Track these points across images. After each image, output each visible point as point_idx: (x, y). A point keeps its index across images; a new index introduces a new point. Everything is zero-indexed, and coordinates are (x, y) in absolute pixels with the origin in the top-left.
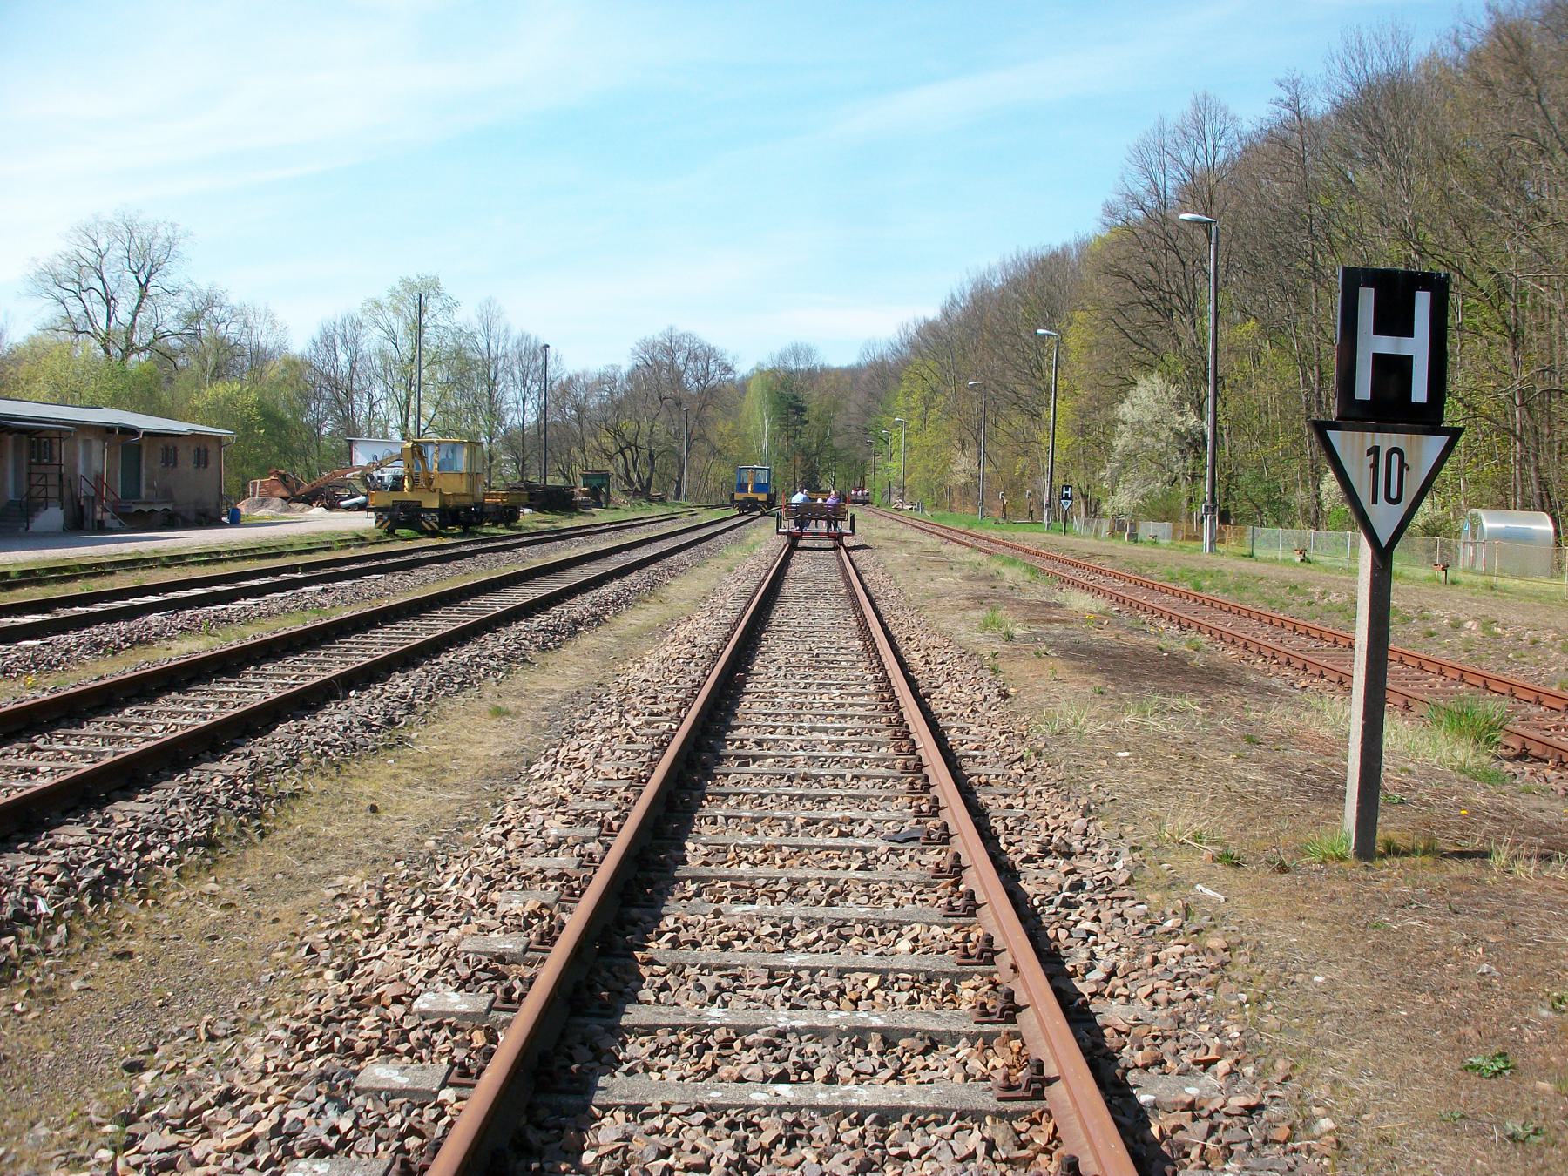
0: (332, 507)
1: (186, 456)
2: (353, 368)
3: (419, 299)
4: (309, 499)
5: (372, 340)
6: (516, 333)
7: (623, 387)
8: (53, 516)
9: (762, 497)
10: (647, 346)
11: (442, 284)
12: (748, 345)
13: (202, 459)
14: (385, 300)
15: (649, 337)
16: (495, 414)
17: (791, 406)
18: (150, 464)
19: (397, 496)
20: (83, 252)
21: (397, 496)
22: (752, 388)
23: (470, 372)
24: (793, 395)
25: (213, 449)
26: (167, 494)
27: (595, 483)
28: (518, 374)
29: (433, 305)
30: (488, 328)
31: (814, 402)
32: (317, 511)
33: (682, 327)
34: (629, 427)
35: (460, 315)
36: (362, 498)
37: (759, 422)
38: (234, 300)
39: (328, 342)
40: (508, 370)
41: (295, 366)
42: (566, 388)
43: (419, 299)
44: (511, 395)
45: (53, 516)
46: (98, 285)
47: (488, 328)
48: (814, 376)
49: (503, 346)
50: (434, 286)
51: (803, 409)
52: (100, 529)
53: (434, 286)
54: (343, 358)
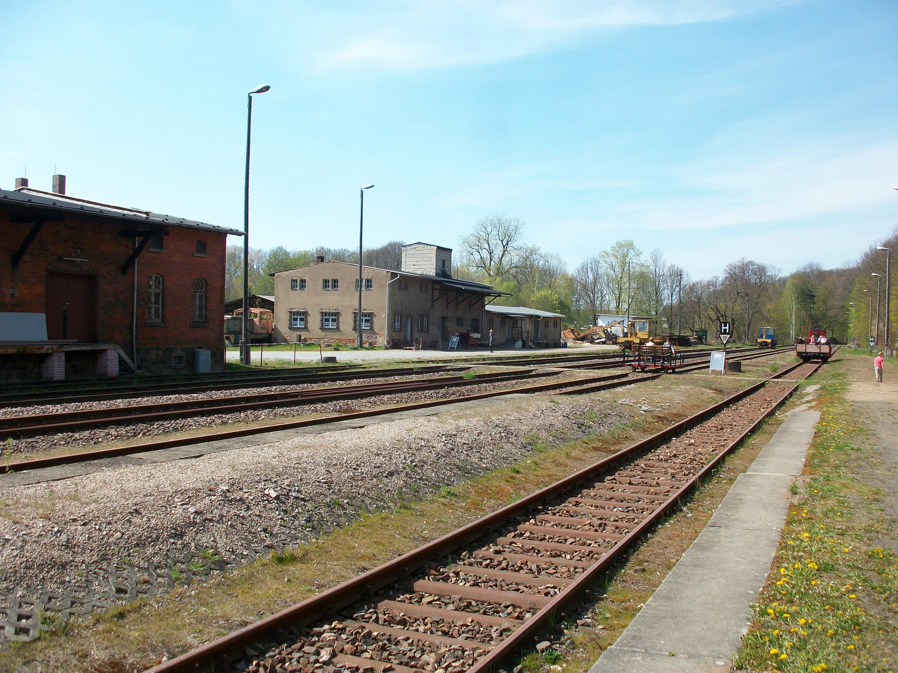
0: (592, 342)
1: (551, 324)
2: (595, 283)
3: (624, 250)
4: (583, 339)
5: (604, 268)
6: (668, 265)
7: (719, 288)
8: (519, 343)
9: (769, 341)
10: (732, 268)
11: (635, 244)
12: (784, 260)
13: (555, 325)
14: (609, 250)
15: (733, 263)
16: (659, 301)
17: (807, 295)
18: (541, 326)
19: (626, 339)
20: (481, 233)
21: (626, 339)
22: (787, 284)
23: (646, 283)
24: (810, 287)
25: (558, 321)
26: (545, 337)
27: (700, 334)
28: (669, 284)
29: (632, 253)
30: (655, 262)
31: (820, 292)
32: (587, 344)
33: (748, 258)
34: (721, 306)
35: (642, 259)
36: (603, 340)
37: (790, 306)
38: (543, 251)
39: (584, 269)
40: (665, 281)
41: (571, 282)
42: (693, 288)
43: (624, 250)
44: (666, 293)
45: (519, 343)
46: (486, 246)
47: (655, 262)
48: (822, 275)
49: (664, 270)
50: (630, 246)
51: (813, 296)
52: (530, 348)
53: (630, 246)
54: (591, 277)
